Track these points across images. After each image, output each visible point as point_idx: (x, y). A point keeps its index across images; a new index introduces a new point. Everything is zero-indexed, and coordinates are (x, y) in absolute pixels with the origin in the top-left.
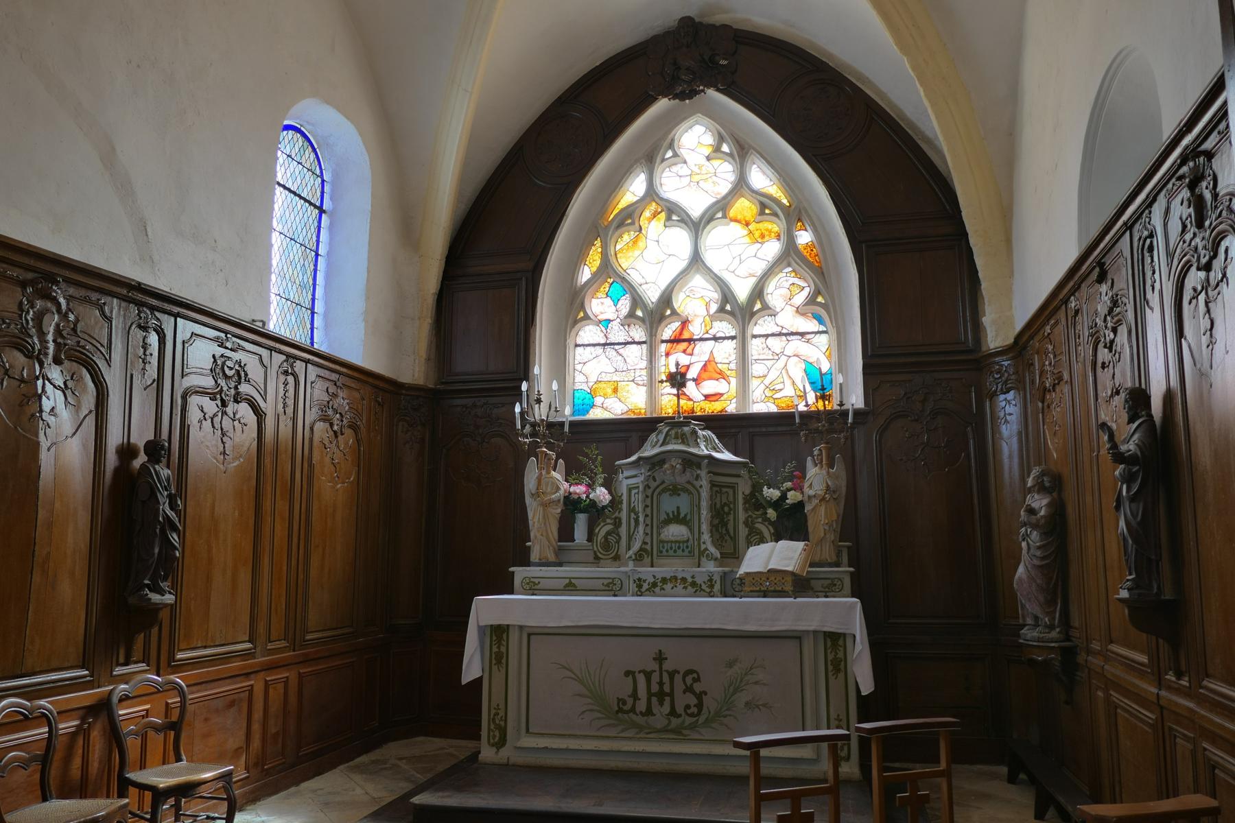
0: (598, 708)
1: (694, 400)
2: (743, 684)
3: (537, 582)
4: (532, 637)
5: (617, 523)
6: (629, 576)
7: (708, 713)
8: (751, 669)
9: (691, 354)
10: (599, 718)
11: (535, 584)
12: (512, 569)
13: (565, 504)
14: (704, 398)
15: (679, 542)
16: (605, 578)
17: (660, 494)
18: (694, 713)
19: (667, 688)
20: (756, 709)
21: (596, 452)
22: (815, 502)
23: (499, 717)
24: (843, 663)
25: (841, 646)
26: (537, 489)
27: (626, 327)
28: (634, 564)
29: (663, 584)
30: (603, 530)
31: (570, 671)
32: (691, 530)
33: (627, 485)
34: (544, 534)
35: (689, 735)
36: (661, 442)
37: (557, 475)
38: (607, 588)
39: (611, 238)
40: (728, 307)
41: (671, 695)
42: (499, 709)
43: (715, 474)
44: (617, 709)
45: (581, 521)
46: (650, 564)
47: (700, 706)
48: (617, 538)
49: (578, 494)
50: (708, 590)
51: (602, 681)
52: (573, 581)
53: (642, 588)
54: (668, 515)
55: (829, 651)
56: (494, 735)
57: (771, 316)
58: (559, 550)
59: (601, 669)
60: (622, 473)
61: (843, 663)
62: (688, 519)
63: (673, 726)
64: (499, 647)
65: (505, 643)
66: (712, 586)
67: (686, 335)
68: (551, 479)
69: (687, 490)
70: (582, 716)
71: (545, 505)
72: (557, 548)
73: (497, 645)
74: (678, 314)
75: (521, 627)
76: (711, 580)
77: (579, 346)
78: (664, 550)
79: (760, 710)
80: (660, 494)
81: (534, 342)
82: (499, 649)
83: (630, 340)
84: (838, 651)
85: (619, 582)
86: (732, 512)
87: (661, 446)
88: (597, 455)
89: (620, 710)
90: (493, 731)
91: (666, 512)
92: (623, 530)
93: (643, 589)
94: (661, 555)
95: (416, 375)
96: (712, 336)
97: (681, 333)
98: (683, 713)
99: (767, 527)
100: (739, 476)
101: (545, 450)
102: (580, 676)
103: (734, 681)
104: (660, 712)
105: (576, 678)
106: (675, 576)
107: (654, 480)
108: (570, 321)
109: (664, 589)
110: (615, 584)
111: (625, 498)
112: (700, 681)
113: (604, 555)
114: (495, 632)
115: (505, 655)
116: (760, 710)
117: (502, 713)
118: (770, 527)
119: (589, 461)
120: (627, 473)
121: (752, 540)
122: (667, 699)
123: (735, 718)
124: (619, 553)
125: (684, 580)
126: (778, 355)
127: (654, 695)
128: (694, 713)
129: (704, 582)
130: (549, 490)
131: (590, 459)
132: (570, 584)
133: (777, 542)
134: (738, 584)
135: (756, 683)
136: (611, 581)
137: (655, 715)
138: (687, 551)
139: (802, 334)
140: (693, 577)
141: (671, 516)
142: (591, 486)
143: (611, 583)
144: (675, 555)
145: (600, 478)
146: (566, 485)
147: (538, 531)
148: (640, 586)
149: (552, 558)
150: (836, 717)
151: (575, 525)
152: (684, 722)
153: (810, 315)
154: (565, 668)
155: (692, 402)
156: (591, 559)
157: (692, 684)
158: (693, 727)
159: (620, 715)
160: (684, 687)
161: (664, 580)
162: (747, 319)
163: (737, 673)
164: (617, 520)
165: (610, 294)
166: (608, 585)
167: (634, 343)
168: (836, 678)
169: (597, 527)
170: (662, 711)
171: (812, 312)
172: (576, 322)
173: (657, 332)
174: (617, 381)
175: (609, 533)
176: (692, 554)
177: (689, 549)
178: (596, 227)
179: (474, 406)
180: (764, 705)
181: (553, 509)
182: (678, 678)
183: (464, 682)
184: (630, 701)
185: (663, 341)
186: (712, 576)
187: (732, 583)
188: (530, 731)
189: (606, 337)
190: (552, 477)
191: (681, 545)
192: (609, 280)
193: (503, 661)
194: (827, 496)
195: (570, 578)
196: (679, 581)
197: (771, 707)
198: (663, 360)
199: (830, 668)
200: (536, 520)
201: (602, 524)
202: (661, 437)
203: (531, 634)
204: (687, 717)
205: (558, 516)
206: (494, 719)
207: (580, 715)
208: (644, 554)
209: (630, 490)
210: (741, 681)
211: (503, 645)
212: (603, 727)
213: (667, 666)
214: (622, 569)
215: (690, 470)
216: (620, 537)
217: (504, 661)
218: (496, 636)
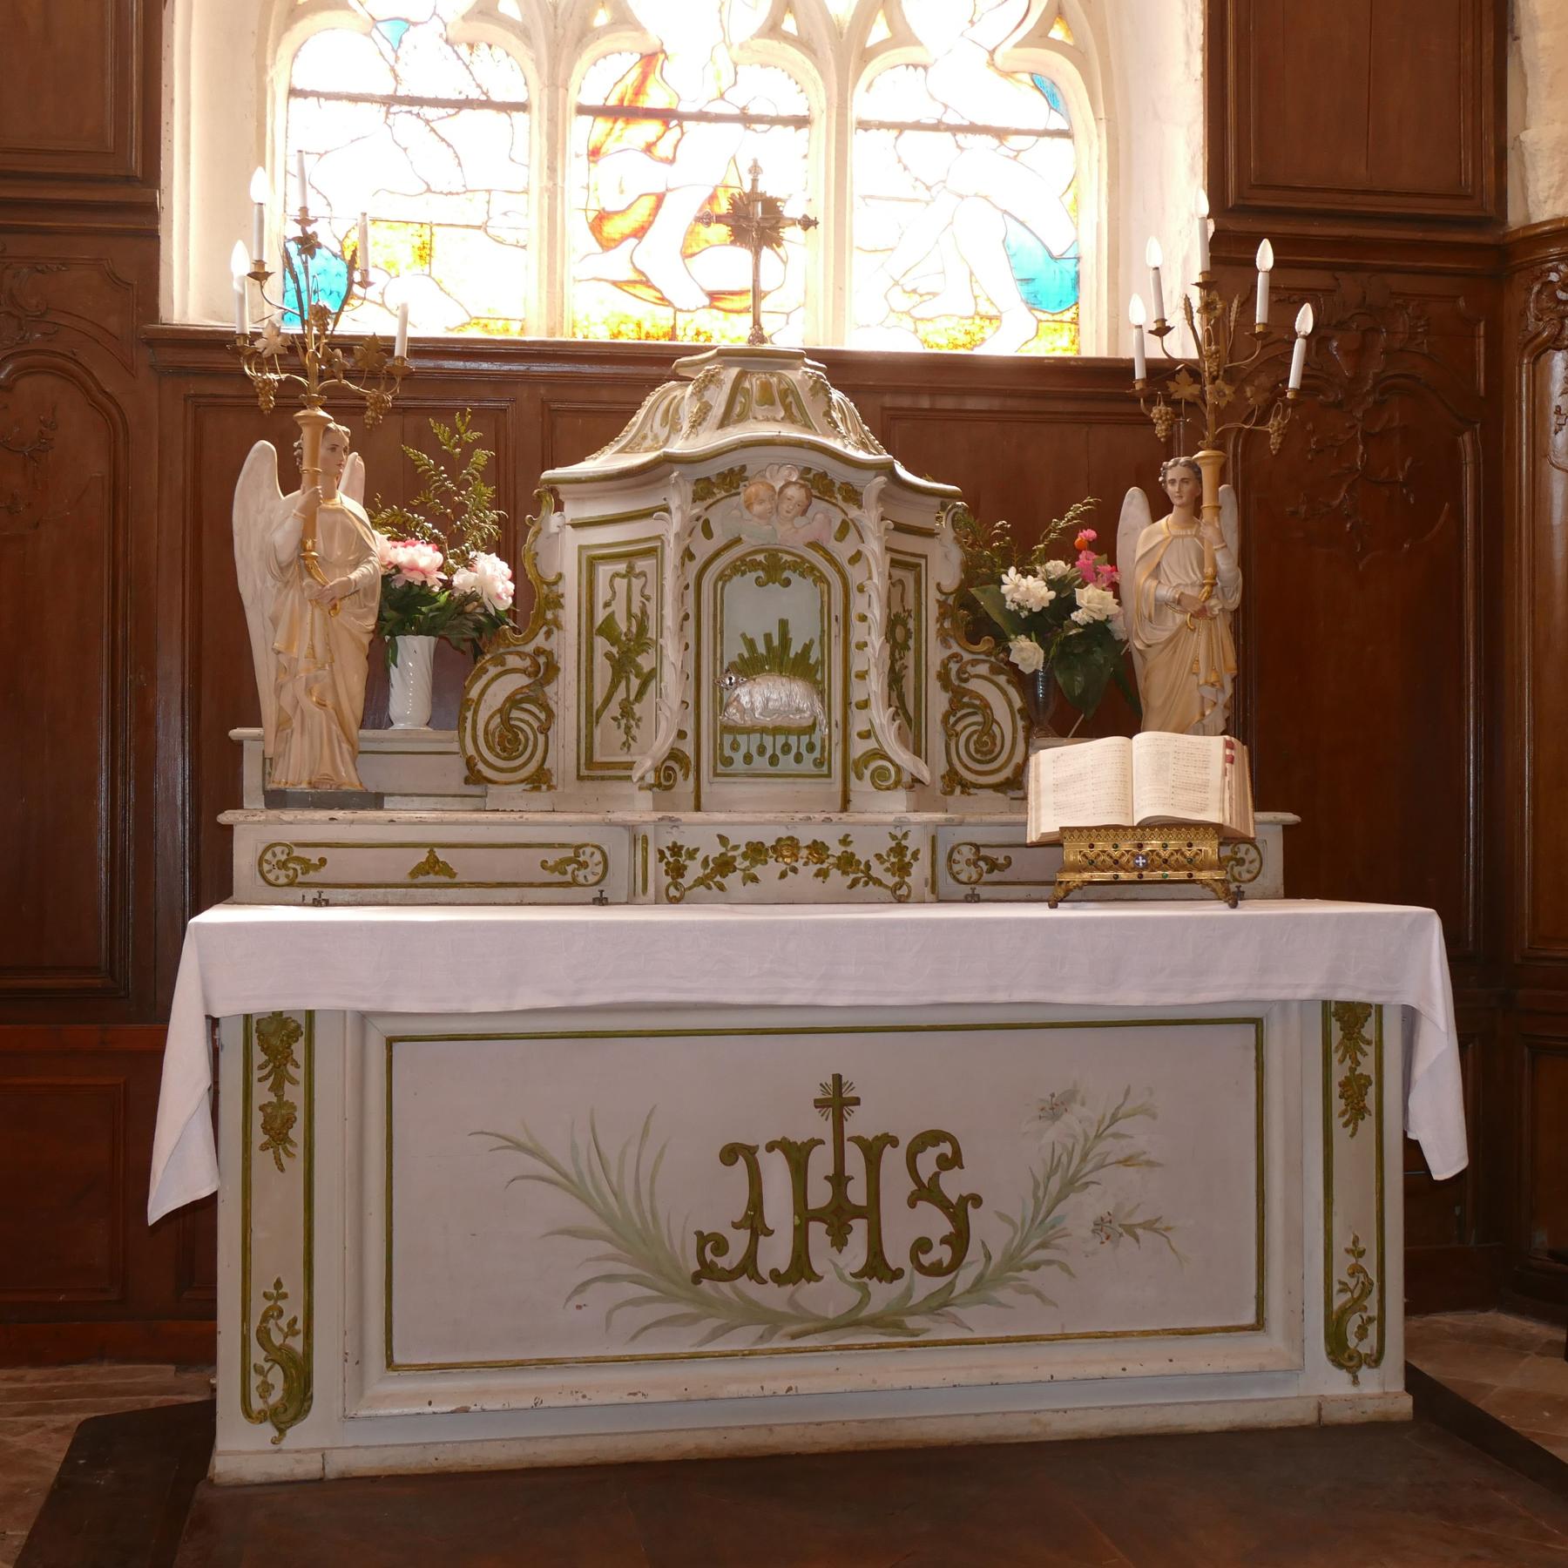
0: (637, 1271)
1: (678, 305)
2: (1089, 1167)
3: (315, 861)
4: (397, 1047)
5: (545, 670)
7: (983, 1260)
8: (1114, 1120)
9: (671, 161)
10: (635, 1302)
11: (307, 866)
14: (707, 301)
15: (787, 731)
16: (551, 846)
17: (723, 578)
18: (940, 1262)
19: (857, 1194)
20: (1127, 1239)
22: (1176, 619)
23: (283, 1322)
24: (1372, 1090)
25: (1369, 1043)
27: (463, 50)
29: (754, 862)
32: (823, 693)
33: (581, 548)
34: (329, 702)
35: (927, 1330)
36: (718, 410)
38: (556, 877)
40: (789, 24)
41: (871, 1212)
42: (285, 1296)
43: (900, 528)
46: (692, 803)
47: (959, 1240)
48: (543, 716)
49: (423, 572)
50: (890, 880)
51: (645, 1187)
52: (441, 855)
53: (682, 876)
54: (750, 644)
55: (1336, 1057)
56: (265, 1383)
57: (915, 66)
59: (642, 1145)
60: (559, 507)
61: (1372, 1090)
62: (812, 661)
63: (875, 1306)
64: (277, 1088)
65: (299, 1074)
66: (903, 869)
67: (654, 98)
68: (339, 517)
69: (813, 568)
70: (577, 1300)
71: (331, 603)
74: (637, 27)
76: (899, 850)
77: (303, 94)
78: (738, 757)
79: (1137, 1240)
80: (723, 578)
82: (280, 1097)
83: (475, 94)
84: (1359, 1056)
85: (598, 857)
86: (911, 643)
87: (723, 423)
89: (706, 1271)
90: (260, 1371)
91: (743, 636)
92: (565, 693)
93: (686, 881)
94: (728, 770)
96: (737, 112)
97: (638, 91)
98: (908, 1266)
99: (1005, 693)
100: (929, 534)
101: (322, 413)
102: (571, 1172)
103: (1064, 1159)
104: (835, 1265)
106: (791, 838)
107: (708, 532)
109: (755, 879)
110: (584, 865)
111: (570, 590)
112: (962, 1167)
113: (501, 770)
115: (300, 1115)
116: (1137, 1240)
117: (293, 1309)
118: (1013, 693)
119: (437, 465)
121: (959, 728)
122: (859, 1227)
123: (1065, 1268)
125: (818, 849)
126: (928, 188)
127: (818, 1216)
128: (940, 1262)
129: (879, 856)
132: (432, 865)
133: (1131, 737)
134: (968, 862)
135: (1127, 1162)
136: (570, 853)
137: (819, 1278)
138: (808, 759)
139: (1000, 134)
140: (845, 841)
141: (761, 649)
143: (569, 861)
144: (772, 770)
145: (489, 522)
147: (309, 692)
148: (677, 871)
149: (349, 778)
150: (1350, 1246)
152: (908, 1293)
153: (1026, 78)
154: (519, 1147)
155: (670, 310)
156: (455, 782)
157: (937, 1175)
158: (938, 1305)
159: (706, 1284)
160: (914, 1187)
161: (756, 851)
162: (852, 66)
163: (1074, 1137)
164: (542, 660)
166: (560, 867)
167: (487, 104)
168: (1352, 1135)
169: (478, 677)
170: (841, 1264)
171: (1032, 68)
173: (569, 75)
174: (431, 225)
175: (513, 701)
176: (825, 768)
177: (817, 754)
180: (1149, 1226)
182: (893, 1160)
183: (155, 1214)
184: (739, 1242)
185: (582, 110)
186: (905, 835)
187: (950, 858)
188: (398, 1359)
189: (396, 76)
191: (793, 740)
194: (1213, 602)
195: (431, 847)
196: (804, 853)
197: (1168, 1229)
198: (575, 168)
199: (1338, 1104)
200: (300, 650)
201: (493, 671)
202: (718, 399)
204: (918, 1276)
206: (264, 1337)
207: (569, 1299)
208: (676, 767)
209: (591, 562)
210: (1084, 1158)
211: (294, 1082)
212: (646, 1328)
213: (860, 1123)
215: (824, 505)
216: (550, 715)
217: (297, 1133)
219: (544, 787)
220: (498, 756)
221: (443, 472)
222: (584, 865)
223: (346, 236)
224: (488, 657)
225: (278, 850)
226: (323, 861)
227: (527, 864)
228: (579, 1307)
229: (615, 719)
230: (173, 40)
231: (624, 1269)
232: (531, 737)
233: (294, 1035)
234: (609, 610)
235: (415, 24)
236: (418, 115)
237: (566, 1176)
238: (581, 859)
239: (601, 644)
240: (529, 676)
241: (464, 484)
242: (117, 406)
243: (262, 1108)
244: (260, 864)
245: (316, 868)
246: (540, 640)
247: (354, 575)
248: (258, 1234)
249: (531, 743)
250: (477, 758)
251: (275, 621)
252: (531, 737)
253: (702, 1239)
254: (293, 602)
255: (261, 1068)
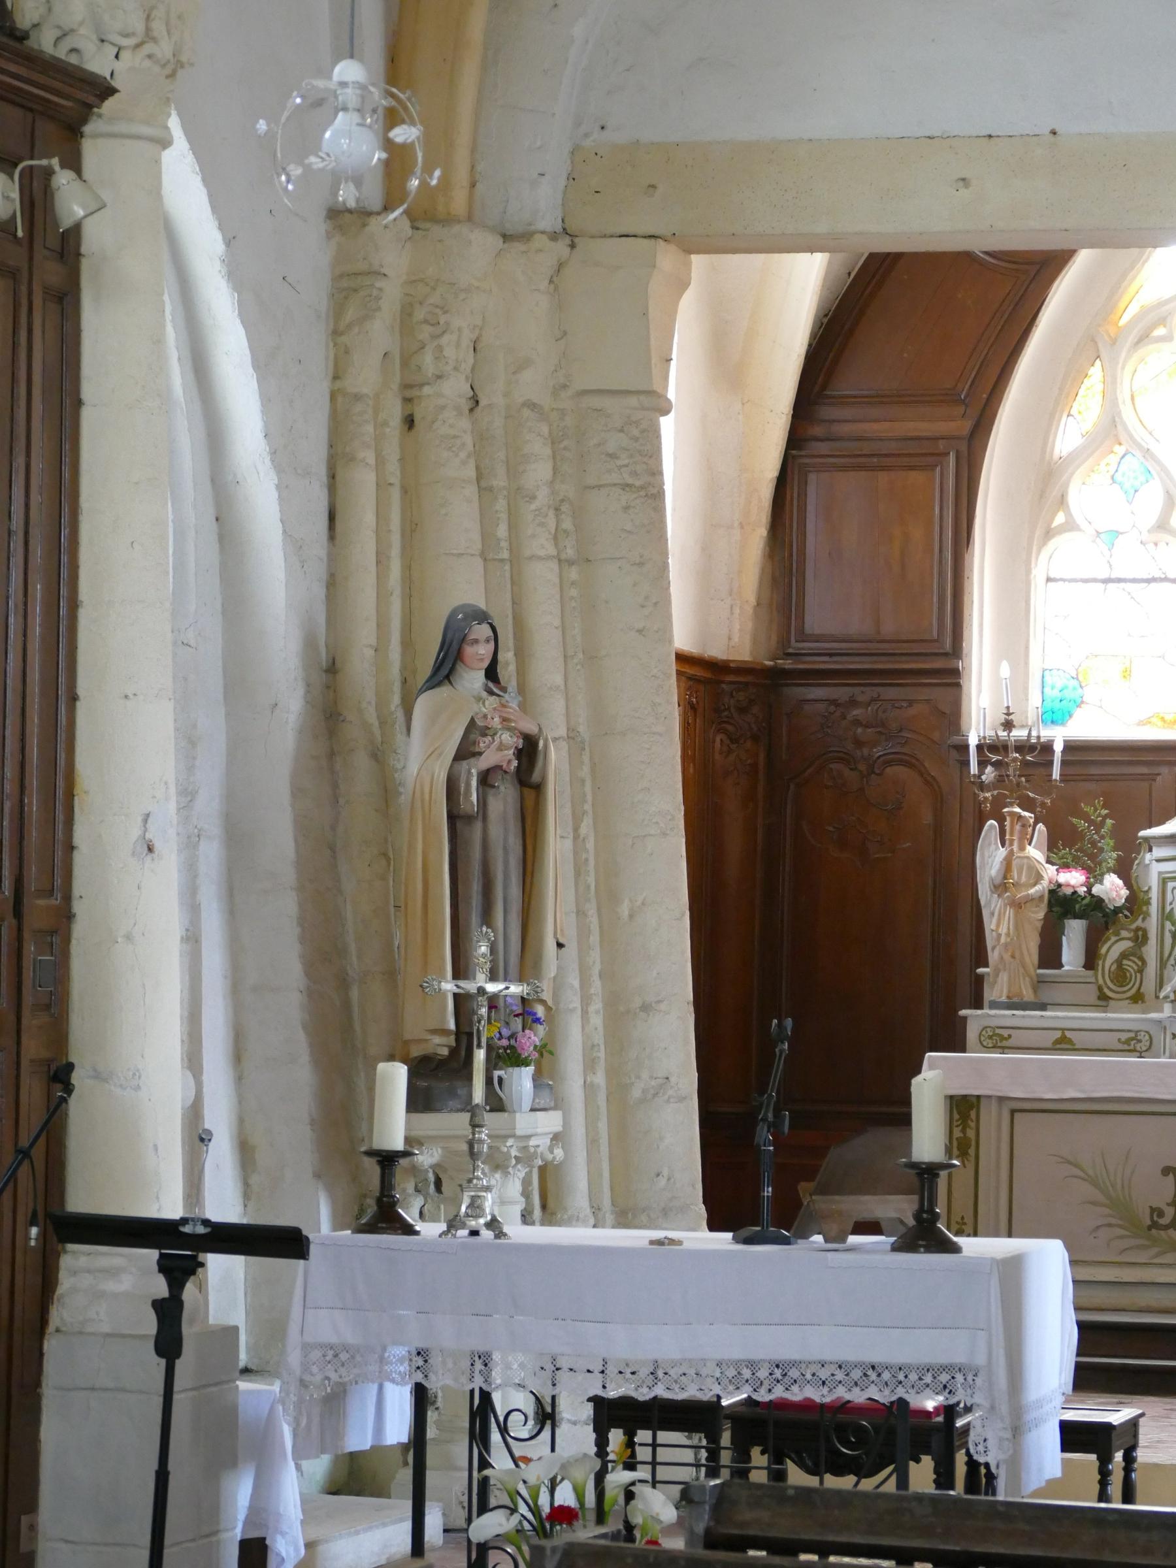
0: (1120, 1222)
4: (1017, 1115)
5: (1141, 938)
6: (1165, 1028)
10: (1122, 1237)
11: (1003, 1038)
12: (963, 1012)
13: (1050, 904)
21: (1105, 812)
26: (1005, 878)
28: (1173, 1008)
30: (1113, 949)
31: (1076, 1166)
33: (1160, 873)
34: (1017, 955)
37: (1035, 853)
38: (1126, 1047)
39: (1123, 368)
42: (965, 1224)
44: (1149, 1223)
45: (1074, 934)
46: (534, 1107)
48: (1140, 963)
49: (1073, 887)
52: (1068, 1034)
58: (1039, 982)
60: (1150, 850)
64: (964, 1131)
65: (973, 1124)
68: (1025, 861)
72: (1035, 979)
73: (960, 1128)
75: (1002, 1099)
81: (971, 594)
83: (1158, 575)
85: (1147, 1037)
88: (1105, 817)
89: (1154, 1225)
92: (1151, 951)
95: (736, 639)
101: (1017, 810)
105: (1086, 1177)
108: (1039, 532)
110: (1140, 1041)
111: (1154, 895)
113: (1118, 993)
114: (957, 1106)
115: (973, 1143)
119: (1089, 827)
120: (1158, 852)
124: (1142, 990)
130: (1023, 879)
131: (1091, 822)
136: (1132, 1035)
142: (1094, 874)
143: (1132, 1039)
145: (1111, 857)
146: (1051, 870)
149: (1028, 995)
151: (1064, 938)
154: (1070, 1163)
156: (1093, 998)
159: (1154, 1231)
164: (1140, 933)
165: (1118, 477)
166: (1127, 1042)
167: (1166, 579)
169: (1105, 942)
172: (1049, 534)
175: (1124, 955)
178: (1094, 341)
179: (853, 703)
181: (1033, 912)
190: (1028, 858)
192: (1117, 448)
193: (970, 1151)
195: (1063, 1030)
200: (1003, 930)
201: (1113, 939)
203: (1017, 1109)
205: (1039, 925)
209: (1164, 882)
214: (1154, 1015)
217: (972, 1151)
218: (959, 1113)
219: (1140, 1002)
220: (1115, 985)
221: (1092, 830)
222: (1140, 1041)
223: (1080, 666)
224: (1111, 931)
225: (988, 1030)
226: (1010, 1036)
227: (1111, 1040)
228: (1095, 1237)
229: (1172, 965)
230: (973, 567)
231: (1113, 1221)
232: (1133, 975)
233: (971, 1107)
234: (1172, 906)
235: (1121, 533)
236: (1124, 589)
237: (1089, 1176)
238: (1139, 1038)
239: (1168, 925)
240: (1132, 941)
241: (1102, 837)
242: (937, 782)
243: (957, 1139)
244: (980, 1037)
245: (1006, 1039)
246: (1139, 923)
247: (1032, 891)
248: (955, 1194)
249: (1133, 978)
250: (1104, 986)
251: (993, 914)
252: (1133, 975)
253: (1152, 1210)
254: (1001, 907)
255: (957, 1121)
